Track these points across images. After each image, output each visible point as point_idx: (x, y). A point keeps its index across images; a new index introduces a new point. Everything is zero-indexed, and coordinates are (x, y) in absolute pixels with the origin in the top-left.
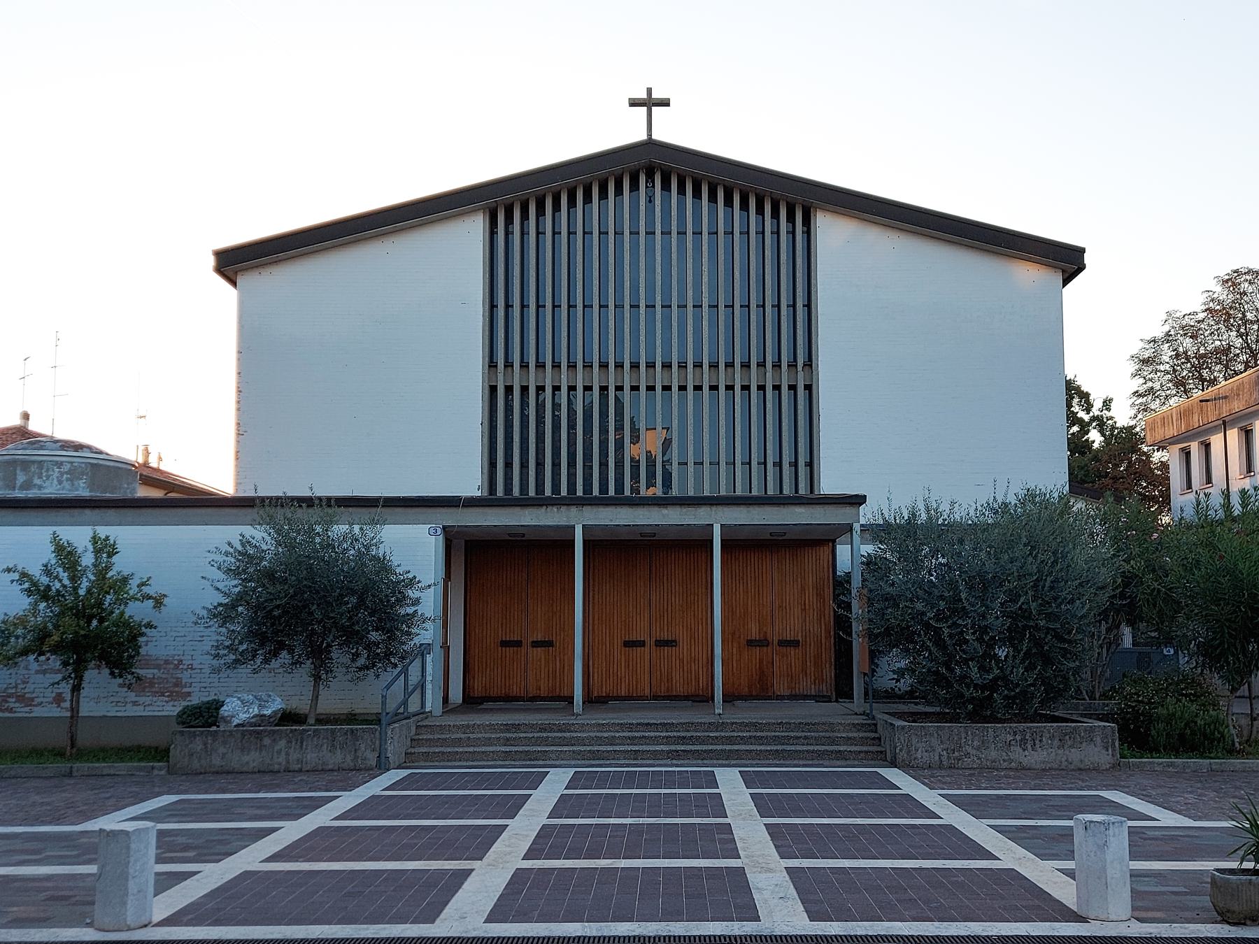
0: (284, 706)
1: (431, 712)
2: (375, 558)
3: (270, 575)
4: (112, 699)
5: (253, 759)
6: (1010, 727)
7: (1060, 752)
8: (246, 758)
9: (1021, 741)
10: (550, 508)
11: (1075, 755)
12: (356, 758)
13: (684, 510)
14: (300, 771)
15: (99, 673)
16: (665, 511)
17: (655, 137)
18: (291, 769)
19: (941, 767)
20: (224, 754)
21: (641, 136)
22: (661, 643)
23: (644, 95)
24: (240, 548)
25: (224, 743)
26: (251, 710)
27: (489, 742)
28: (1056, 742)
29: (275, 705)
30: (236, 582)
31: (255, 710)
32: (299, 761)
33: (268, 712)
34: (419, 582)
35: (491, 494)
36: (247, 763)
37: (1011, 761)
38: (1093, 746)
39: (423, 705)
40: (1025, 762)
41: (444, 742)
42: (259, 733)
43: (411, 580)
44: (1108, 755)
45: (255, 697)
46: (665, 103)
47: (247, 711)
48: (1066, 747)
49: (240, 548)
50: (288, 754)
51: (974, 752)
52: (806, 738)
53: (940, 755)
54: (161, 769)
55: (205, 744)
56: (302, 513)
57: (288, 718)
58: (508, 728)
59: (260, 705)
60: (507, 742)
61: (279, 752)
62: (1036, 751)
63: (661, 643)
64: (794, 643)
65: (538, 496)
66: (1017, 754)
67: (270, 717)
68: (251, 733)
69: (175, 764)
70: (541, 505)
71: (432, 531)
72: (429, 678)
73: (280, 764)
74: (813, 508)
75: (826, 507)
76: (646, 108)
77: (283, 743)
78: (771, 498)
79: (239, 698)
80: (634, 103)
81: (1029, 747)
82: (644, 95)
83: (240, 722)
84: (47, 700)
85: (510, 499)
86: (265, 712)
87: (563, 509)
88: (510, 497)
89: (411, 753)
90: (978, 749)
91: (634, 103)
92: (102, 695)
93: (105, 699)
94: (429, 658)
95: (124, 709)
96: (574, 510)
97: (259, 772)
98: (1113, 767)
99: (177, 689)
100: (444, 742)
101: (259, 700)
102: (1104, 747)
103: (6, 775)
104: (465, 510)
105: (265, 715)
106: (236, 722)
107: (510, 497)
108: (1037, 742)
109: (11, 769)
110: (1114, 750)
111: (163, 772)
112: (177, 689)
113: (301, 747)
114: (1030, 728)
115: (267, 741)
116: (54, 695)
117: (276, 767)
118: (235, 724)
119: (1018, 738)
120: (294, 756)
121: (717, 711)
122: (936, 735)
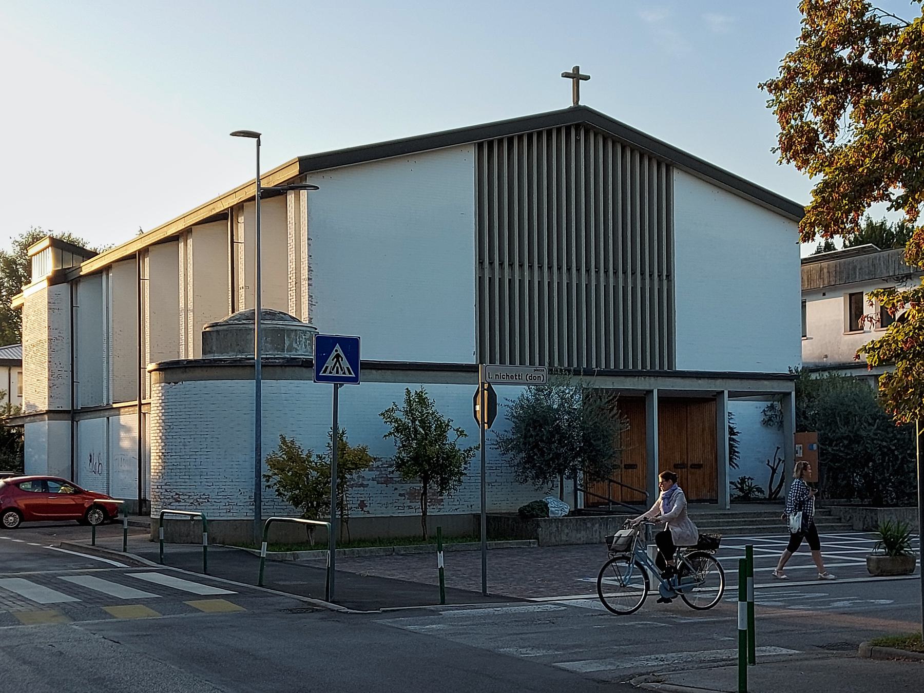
4: (396, 504)
8: (579, 535)
10: (640, 378)
13: (710, 381)
15: (387, 486)
17: (581, 103)
20: (568, 533)
21: (568, 104)
22: (628, 467)
36: (580, 538)
46: (586, 78)
50: (600, 532)
54: (534, 544)
55: (558, 527)
63: (628, 467)
64: (699, 466)
65: (210, 357)
69: (542, 540)
70: (635, 376)
73: (596, 538)
74: (202, 371)
75: (779, 381)
78: (621, 371)
80: (566, 75)
84: (355, 506)
90: (911, 520)
91: (566, 75)
92: (389, 502)
93: (391, 505)
95: (403, 511)
97: (586, 544)
99: (435, 497)
103: (450, 550)
104: (599, 378)
109: (452, 546)
111: (536, 546)
112: (435, 497)
116: (359, 502)
117: (595, 541)
121: (727, 507)
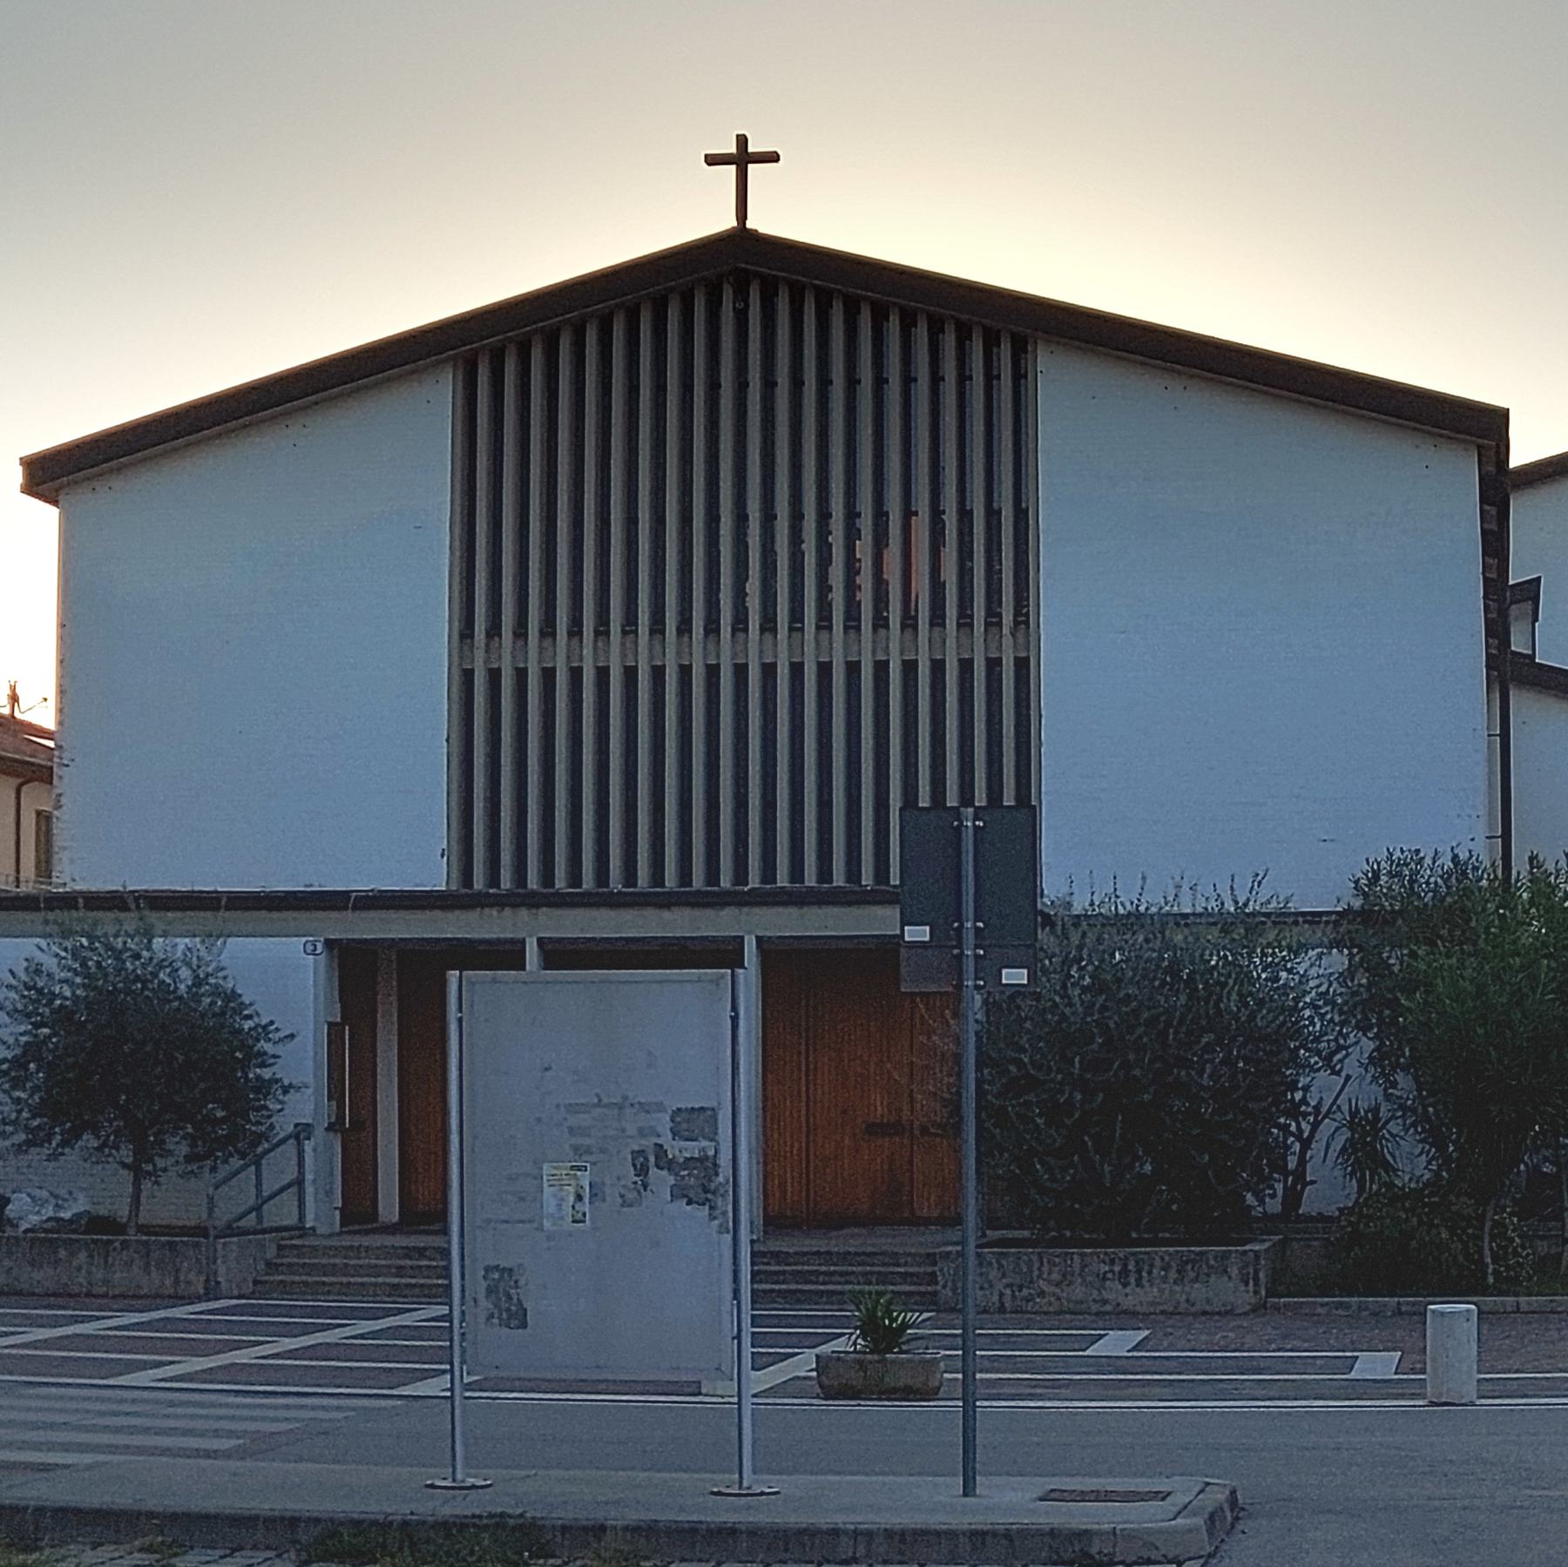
0: (87, 1208)
1: (313, 1229)
2: (217, 991)
3: (64, 1017)
5: (44, 1277)
6: (1106, 1254)
7: (1177, 1288)
8: (38, 1275)
9: (1120, 1273)
10: (487, 910)
11: (1199, 1292)
12: (177, 1282)
14: (105, 1296)
16: (667, 915)
17: (750, 224)
18: (94, 1292)
19: (1002, 1309)
23: (732, 149)
24: (24, 977)
25: (10, 1253)
26: (43, 1212)
27: (376, 1271)
28: (1173, 1275)
29: (80, 1205)
30: (23, 1028)
31: (49, 1212)
32: (106, 1282)
33: (66, 1215)
34: (277, 1030)
35: (709, 883)
37: (1105, 1302)
38: (1226, 1278)
39: (302, 1217)
40: (1128, 1303)
41: (311, 1269)
42: (51, 1241)
43: (265, 1027)
44: (1248, 1292)
45: (51, 1194)
47: (38, 1213)
48: (1186, 1281)
49: (24, 977)
51: (1052, 1289)
52: (842, 1274)
53: (1001, 1295)
56: (107, 922)
57: (98, 1224)
58: (408, 1252)
59: (57, 1205)
60: (400, 1270)
61: (79, 1269)
62: (1143, 1287)
66: (1113, 1291)
67: (71, 1221)
68: (42, 1241)
71: (310, 948)
72: (309, 1177)
76: (750, 166)
77: (82, 1256)
79: (29, 1195)
81: (1132, 1280)
82: (732, 149)
83: (29, 1226)
85: (714, 892)
86: (62, 1215)
87: (508, 911)
88: (716, 889)
89: (261, 1282)
90: (1058, 1285)
94: (308, 1146)
96: (523, 913)
98: (1254, 1310)
100: (311, 1269)
101: (56, 1197)
102: (1242, 1280)
105: (62, 1219)
106: (24, 1226)
107: (716, 889)
108: (1144, 1274)
110: (1256, 1284)
113: (106, 1262)
114: (1134, 1254)
115: (63, 1253)
117: (76, 1290)
118: (22, 1228)
119: (1117, 1268)
120: (99, 1275)
122: (995, 1265)
